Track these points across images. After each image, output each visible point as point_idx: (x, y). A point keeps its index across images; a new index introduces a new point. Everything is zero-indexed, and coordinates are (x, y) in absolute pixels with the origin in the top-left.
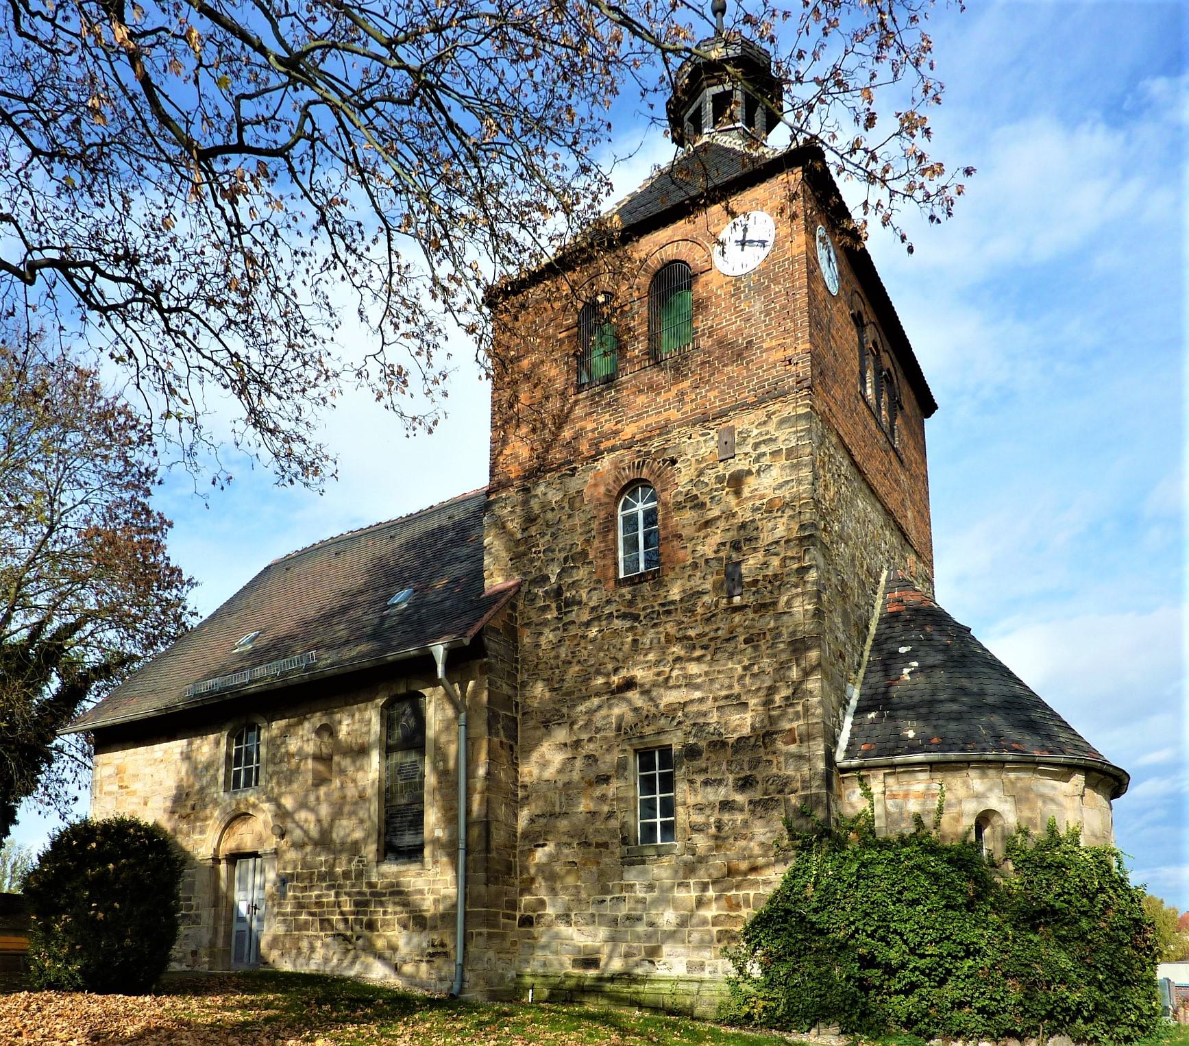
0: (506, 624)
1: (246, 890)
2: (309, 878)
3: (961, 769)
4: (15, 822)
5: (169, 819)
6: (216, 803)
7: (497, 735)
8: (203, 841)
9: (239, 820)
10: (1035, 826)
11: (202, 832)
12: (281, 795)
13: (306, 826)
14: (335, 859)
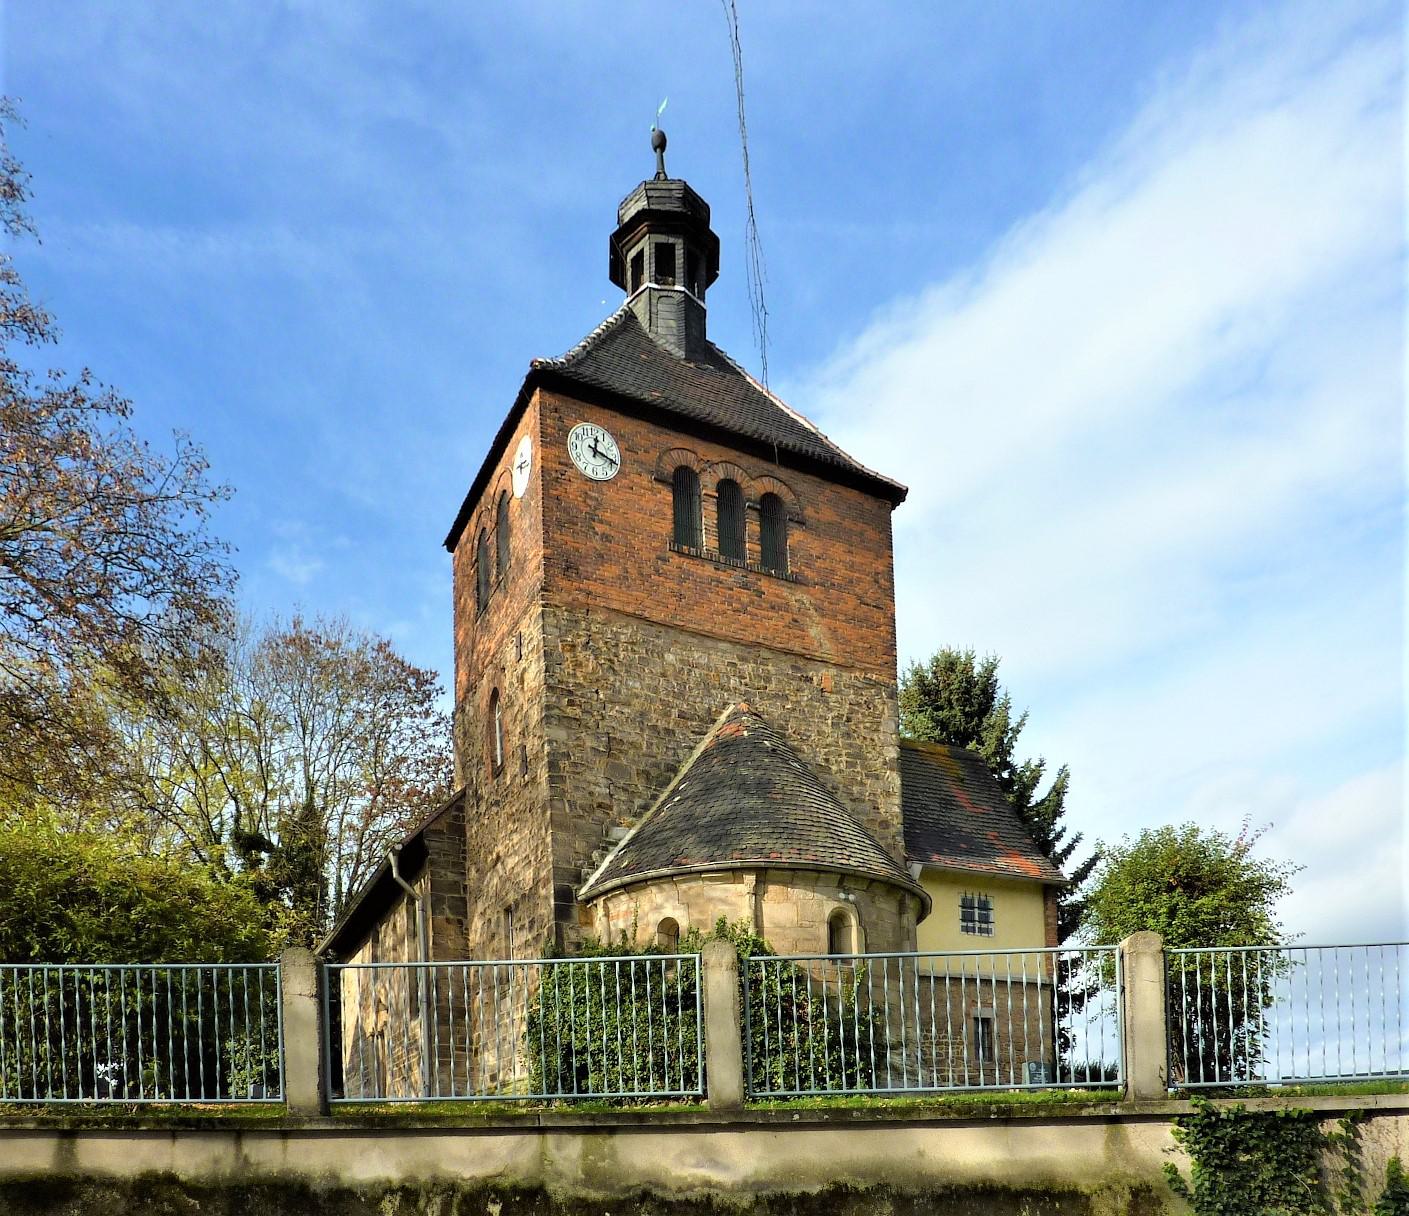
0: (450, 825)
3: (644, 888)
4: (1145, 836)
7: (442, 912)
10: (705, 927)
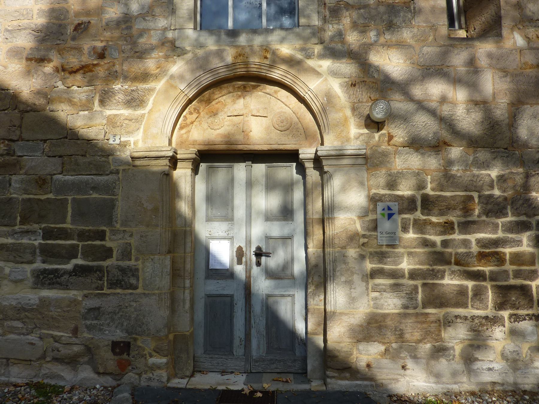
1: (229, 218)
2: (462, 207)
5: (28, 73)
6: (174, 49)
8: (138, 120)
9: (228, 87)
11: (134, 101)
12: (367, 47)
13: (445, 110)
14: (527, 176)
